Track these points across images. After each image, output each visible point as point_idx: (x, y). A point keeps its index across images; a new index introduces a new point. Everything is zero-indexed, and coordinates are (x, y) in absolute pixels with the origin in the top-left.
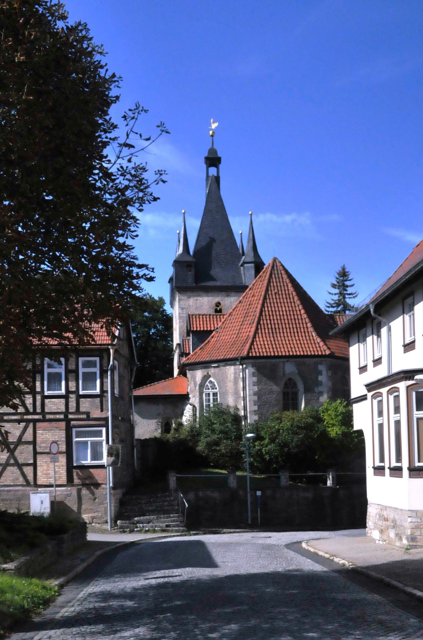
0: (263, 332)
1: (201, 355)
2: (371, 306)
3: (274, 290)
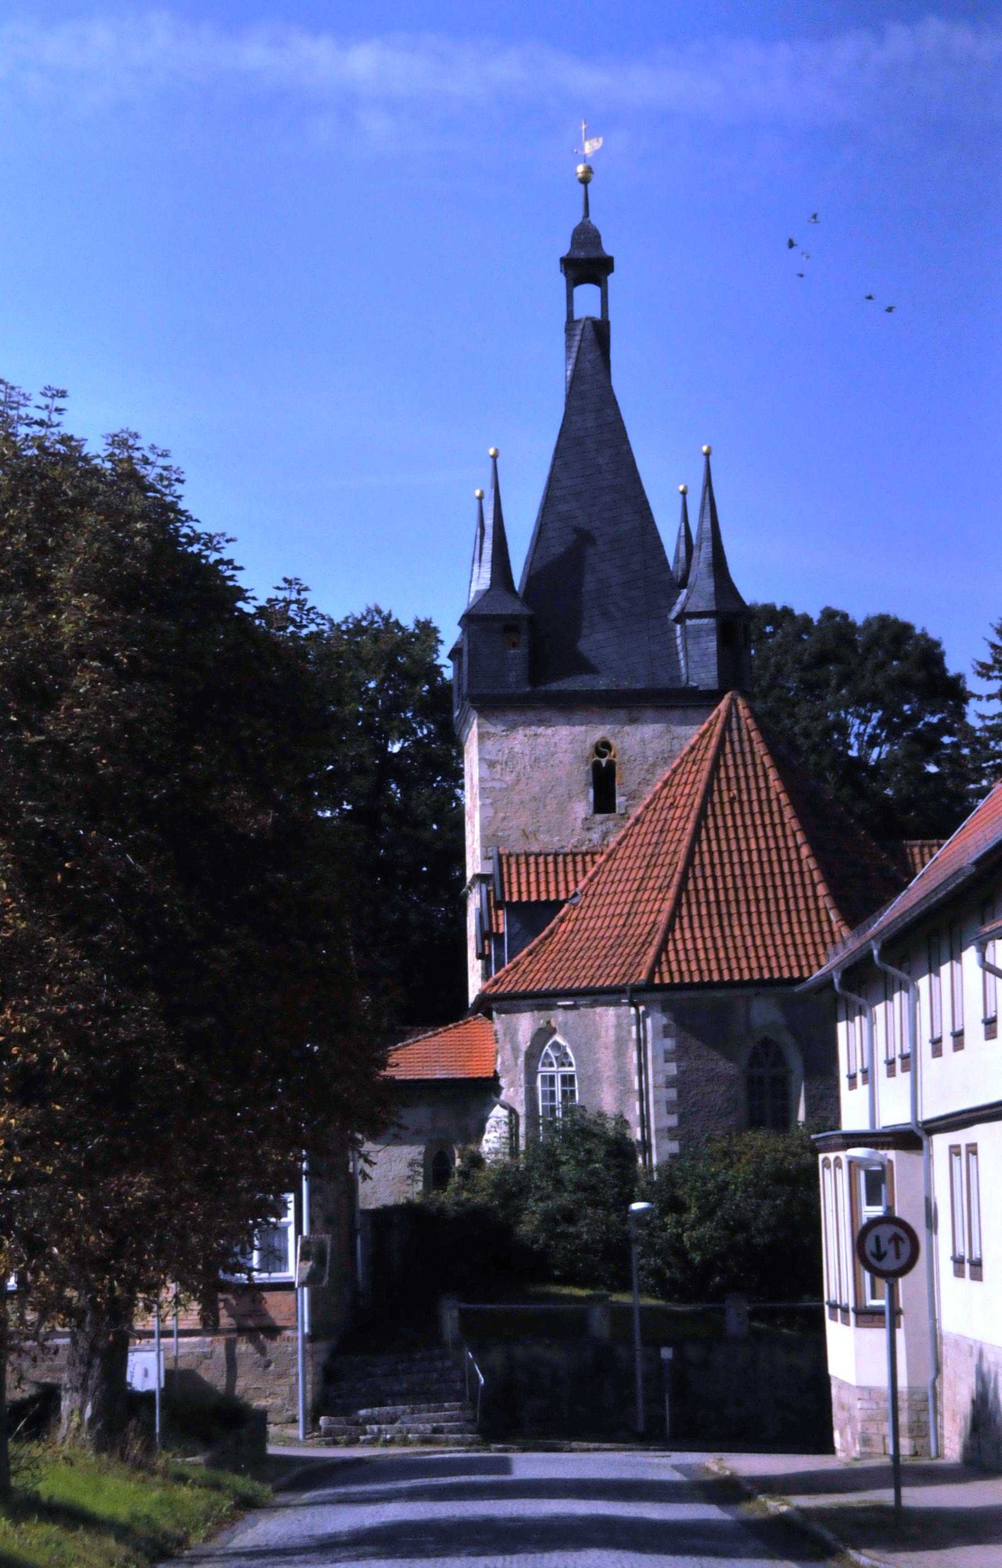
0: (694, 912)
1: (531, 971)
2: (834, 973)
3: (729, 790)
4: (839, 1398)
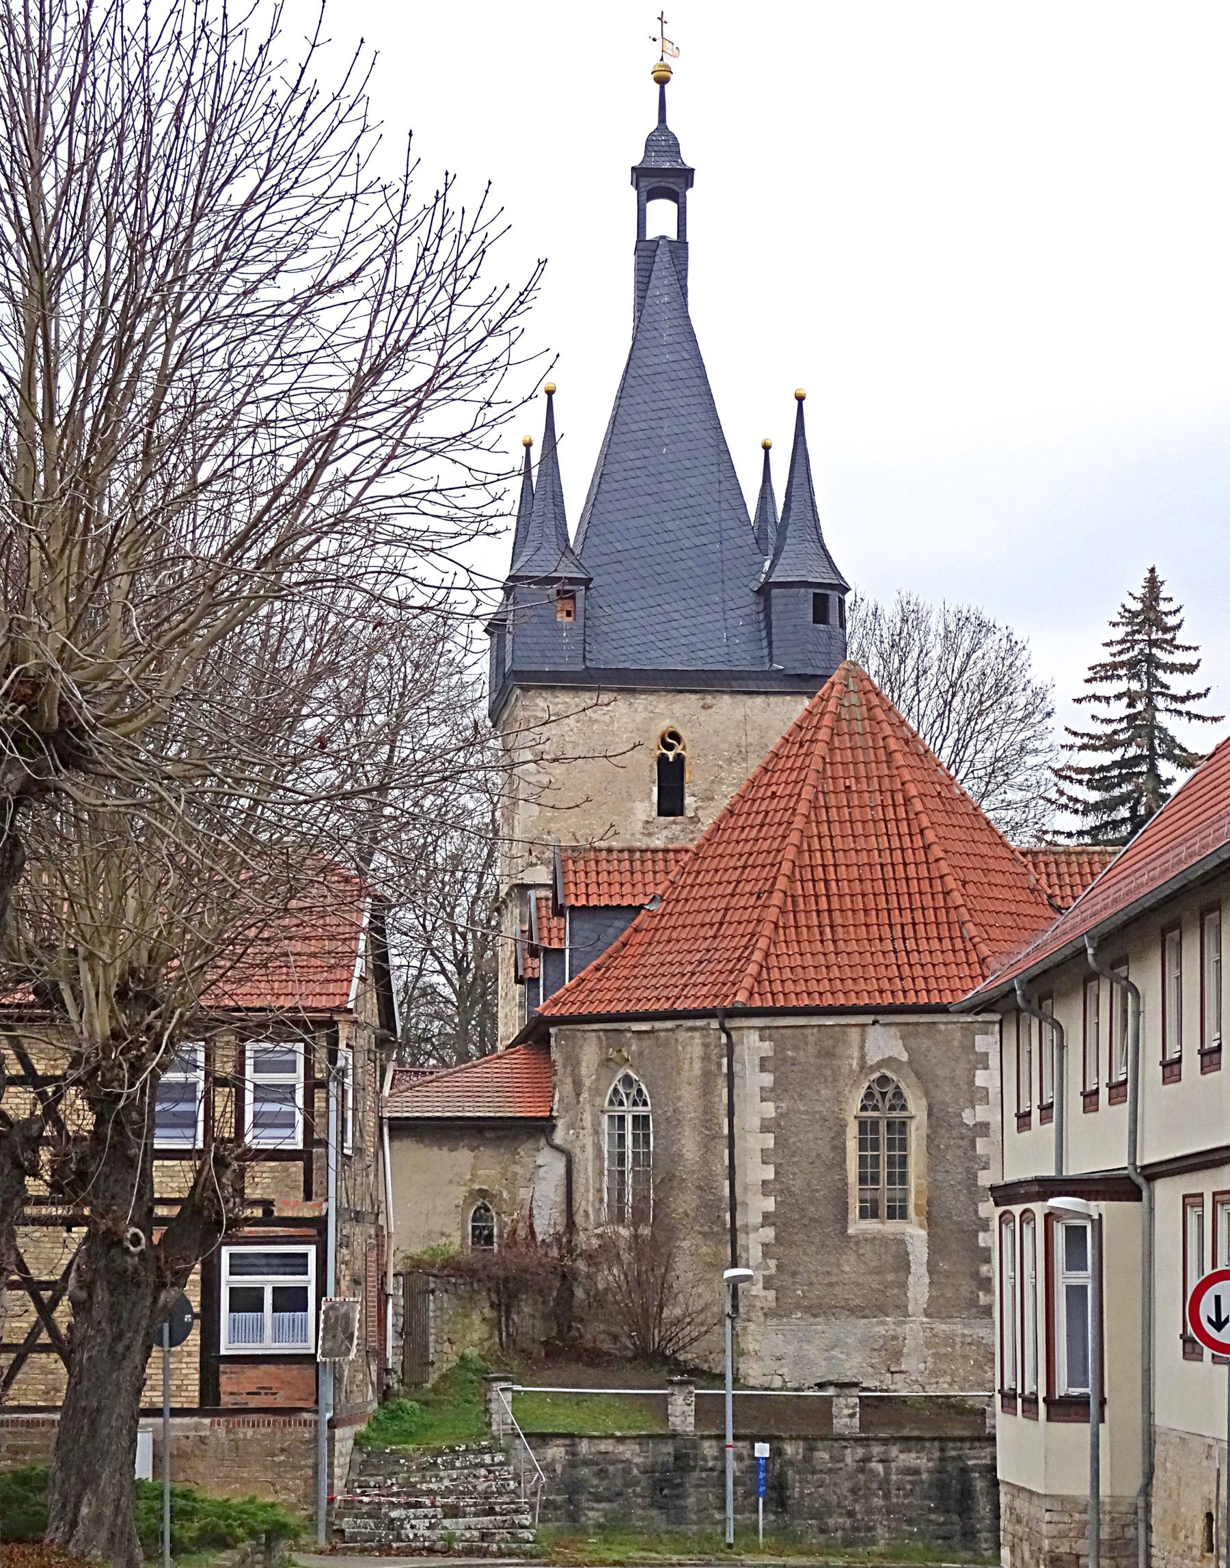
4: (1012, 1509)
